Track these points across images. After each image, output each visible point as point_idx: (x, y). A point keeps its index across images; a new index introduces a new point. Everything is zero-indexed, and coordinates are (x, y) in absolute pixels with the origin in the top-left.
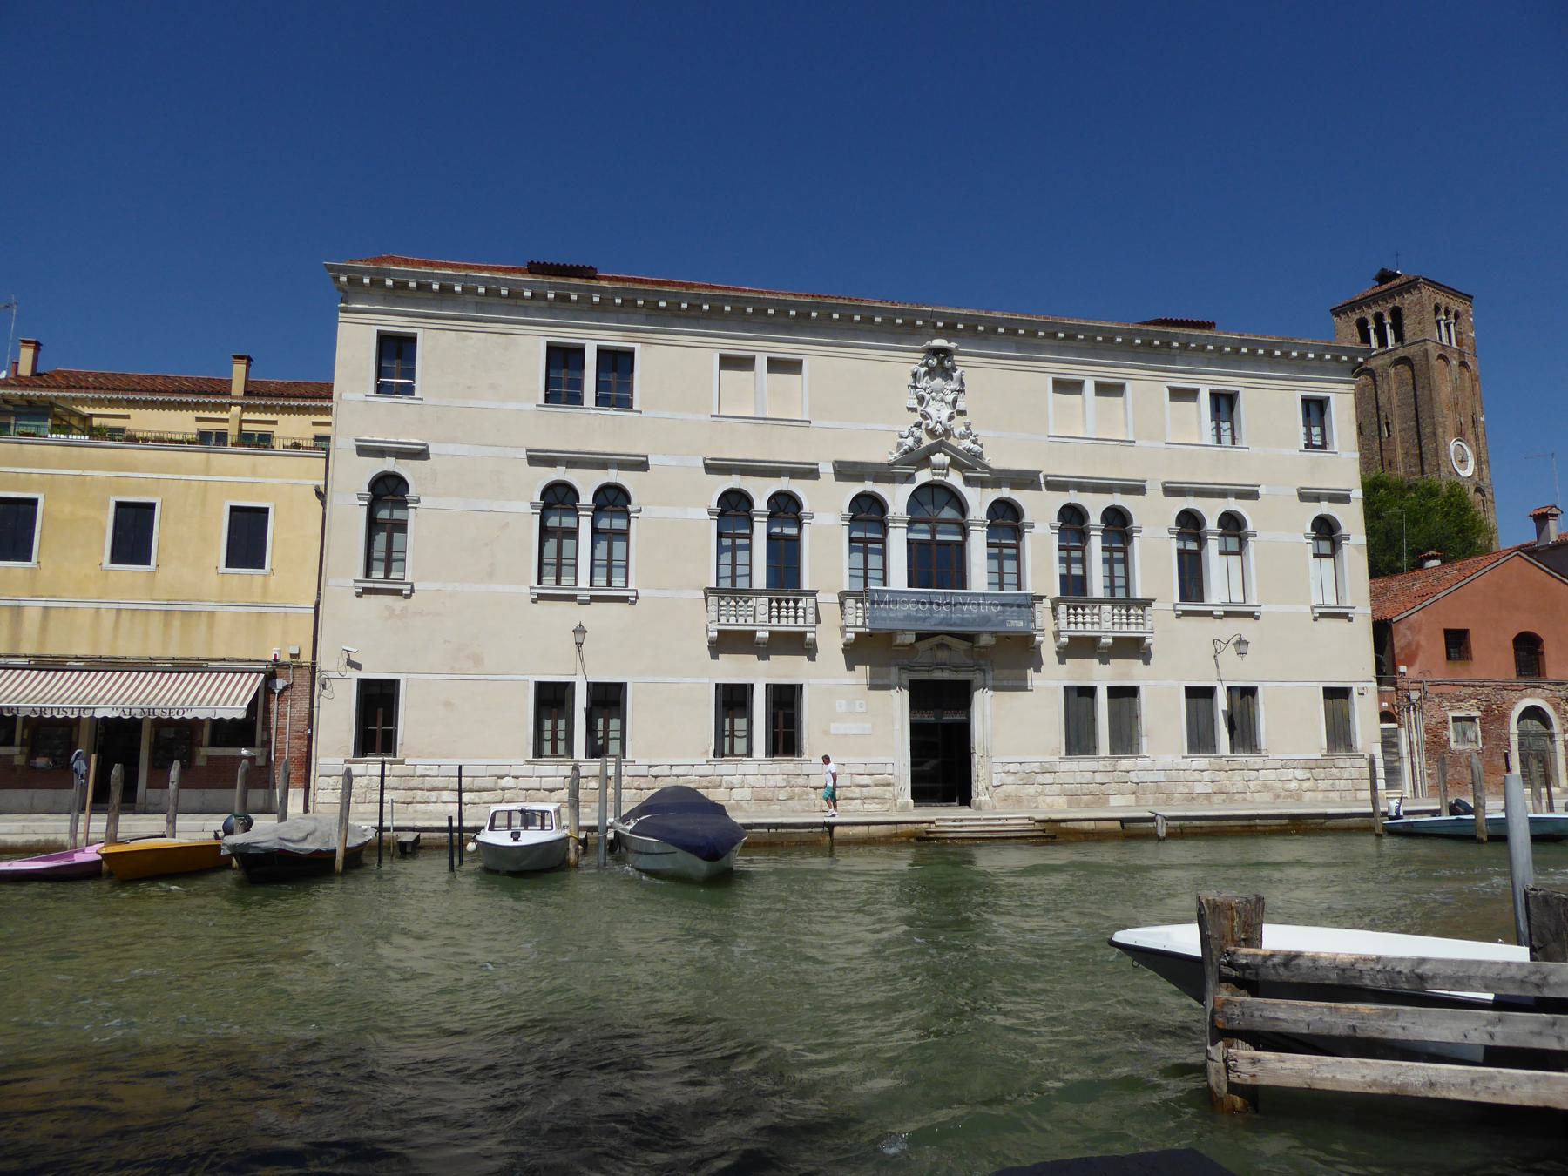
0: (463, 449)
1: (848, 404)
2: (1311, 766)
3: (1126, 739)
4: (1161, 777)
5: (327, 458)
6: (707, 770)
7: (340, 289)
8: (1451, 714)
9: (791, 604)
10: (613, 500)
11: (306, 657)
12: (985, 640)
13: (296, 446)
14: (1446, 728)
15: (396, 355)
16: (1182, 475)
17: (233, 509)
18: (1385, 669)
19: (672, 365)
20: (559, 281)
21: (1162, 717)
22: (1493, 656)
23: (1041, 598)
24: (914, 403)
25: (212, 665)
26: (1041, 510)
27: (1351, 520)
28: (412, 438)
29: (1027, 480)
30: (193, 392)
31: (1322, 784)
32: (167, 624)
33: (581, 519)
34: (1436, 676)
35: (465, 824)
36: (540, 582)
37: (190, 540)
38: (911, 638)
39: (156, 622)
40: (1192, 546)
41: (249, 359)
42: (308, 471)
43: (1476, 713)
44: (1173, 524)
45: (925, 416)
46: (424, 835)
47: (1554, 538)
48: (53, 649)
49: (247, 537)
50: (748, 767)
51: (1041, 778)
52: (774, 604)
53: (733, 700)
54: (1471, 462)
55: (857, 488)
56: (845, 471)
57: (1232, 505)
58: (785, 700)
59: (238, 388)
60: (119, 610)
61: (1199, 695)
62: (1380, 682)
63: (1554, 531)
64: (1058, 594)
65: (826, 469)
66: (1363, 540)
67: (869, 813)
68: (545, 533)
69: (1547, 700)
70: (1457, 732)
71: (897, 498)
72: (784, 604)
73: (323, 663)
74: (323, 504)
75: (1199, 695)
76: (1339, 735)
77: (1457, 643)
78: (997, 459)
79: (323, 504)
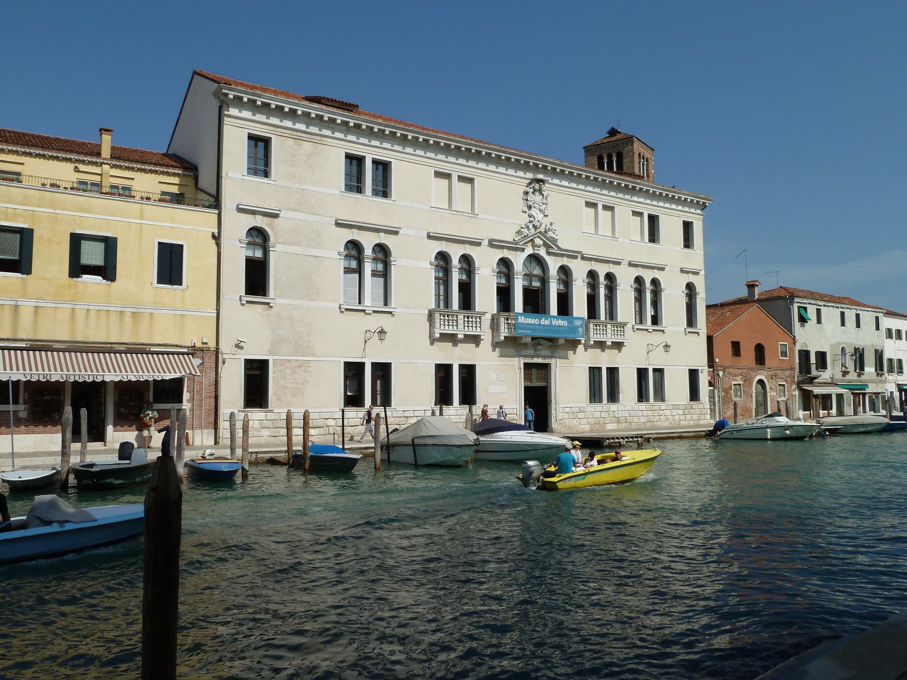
3: (613, 396)
4: (626, 414)
8: (733, 383)
10: (382, 251)
11: (212, 345)
12: (562, 341)
13: (148, 199)
15: (260, 146)
16: (636, 259)
17: (182, 246)
19: (412, 170)
20: (333, 106)
21: (628, 384)
22: (748, 352)
23: (484, 313)
24: (526, 209)
25: (153, 349)
26: (580, 271)
28: (270, 205)
29: (573, 255)
31: (688, 417)
34: (728, 364)
35: (346, 447)
37: (137, 263)
40: (259, 254)
42: (204, 220)
43: (741, 382)
44: (342, 249)
46: (259, 456)
47: (757, 297)
48: (44, 334)
49: (170, 265)
51: (579, 415)
56: (492, 244)
58: (468, 372)
59: (106, 152)
61: (642, 374)
64: (433, 307)
65: (486, 243)
71: (518, 260)
73: (223, 348)
74: (218, 245)
76: (694, 395)
77: (736, 347)
78: (564, 244)
79: (218, 245)
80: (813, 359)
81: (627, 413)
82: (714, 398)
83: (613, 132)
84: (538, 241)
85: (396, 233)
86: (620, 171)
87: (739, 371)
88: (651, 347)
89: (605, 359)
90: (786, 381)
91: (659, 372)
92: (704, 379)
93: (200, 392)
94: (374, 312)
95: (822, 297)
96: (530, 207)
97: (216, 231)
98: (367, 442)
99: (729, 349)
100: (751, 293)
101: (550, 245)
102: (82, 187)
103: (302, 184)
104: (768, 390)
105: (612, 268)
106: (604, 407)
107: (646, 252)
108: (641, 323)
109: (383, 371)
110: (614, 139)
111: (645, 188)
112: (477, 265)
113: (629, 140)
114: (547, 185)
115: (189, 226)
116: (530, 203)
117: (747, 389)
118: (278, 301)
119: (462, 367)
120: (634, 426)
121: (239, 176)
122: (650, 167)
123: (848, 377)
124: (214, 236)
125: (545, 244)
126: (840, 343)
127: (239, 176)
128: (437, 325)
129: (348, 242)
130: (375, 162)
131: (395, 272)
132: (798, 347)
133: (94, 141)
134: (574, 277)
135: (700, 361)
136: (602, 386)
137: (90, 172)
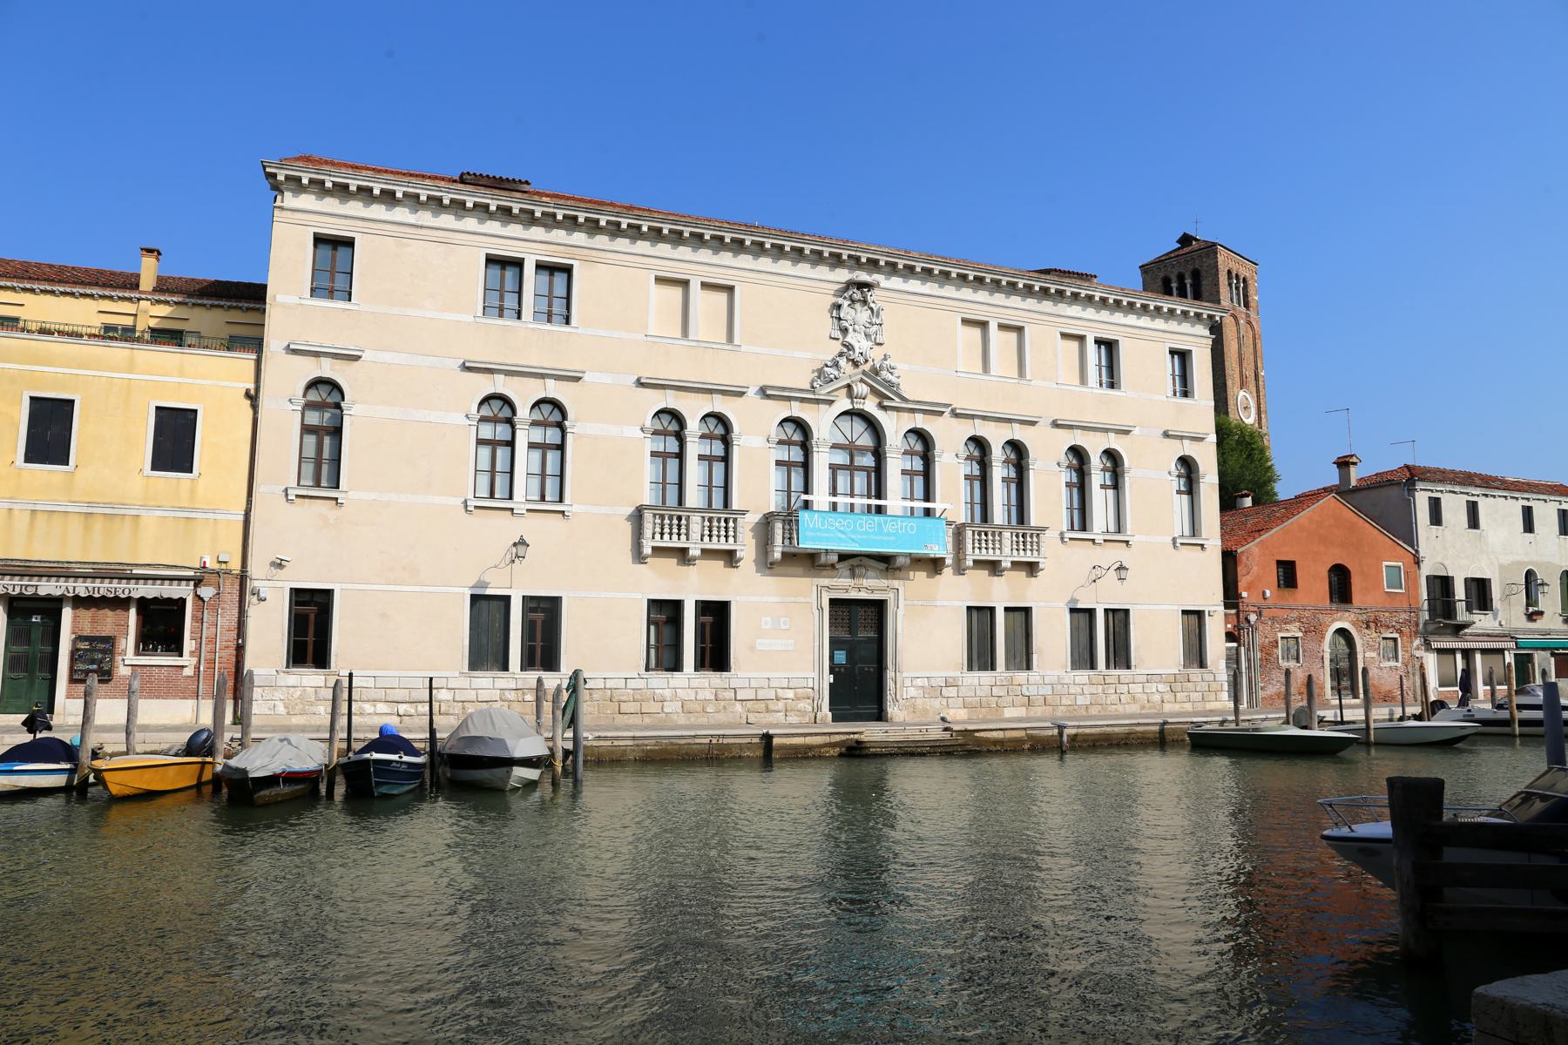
2: (1173, 682)
3: (1023, 657)
4: (1047, 691)
5: (258, 362)
6: (641, 684)
8: (1280, 635)
10: (554, 412)
11: (235, 565)
12: (900, 561)
18: (1231, 595)
19: (619, 283)
20: (495, 189)
21: (1053, 636)
22: (1314, 582)
24: (838, 334)
26: (950, 441)
27: (1207, 460)
29: (934, 411)
30: (97, 284)
32: (87, 528)
33: (522, 434)
37: (112, 440)
39: (76, 524)
42: (235, 368)
43: (1300, 634)
45: (850, 347)
47: (1353, 483)
49: (174, 440)
50: (677, 679)
51: (948, 692)
53: (665, 614)
54: (1253, 411)
57: (553, 390)
58: (716, 615)
59: (147, 283)
60: (33, 512)
61: (1083, 616)
62: (1226, 607)
63: (1355, 474)
64: (647, 496)
65: (752, 391)
67: (791, 725)
69: (1354, 624)
71: (823, 423)
74: (255, 407)
75: (1083, 616)
76: (1196, 654)
77: (1288, 574)
79: (255, 407)
80: (1460, 592)
81: (1053, 690)
82: (1238, 662)
83: (1186, 240)
84: (861, 389)
85: (1127, 432)
86: (1197, 296)
87: (1295, 614)
88: (1098, 572)
89: (1001, 593)
90: (1400, 632)
92: (1215, 629)
93: (213, 640)
95: (1467, 479)
96: (845, 331)
97: (252, 386)
98: (825, 724)
99: (1272, 574)
100: (1345, 477)
101: (886, 393)
102: (110, 333)
103: (412, 305)
104: (1359, 648)
105: (1019, 433)
106: (690, 681)
107: (1093, 403)
108: (1084, 528)
109: (1119, 619)
110: (1186, 250)
111: (1083, 293)
112: (1126, 463)
113: (1211, 248)
114: (876, 292)
115: (205, 379)
116: (845, 324)
117: (1312, 645)
121: (470, 318)
122: (1251, 291)
123: (1539, 624)
124: (247, 395)
125: (874, 391)
126: (1520, 563)
127: (296, 300)
128: (648, 532)
130: (1099, 342)
131: (1128, 480)
132: (1426, 570)
133: (128, 269)
134: (1202, 470)
135: (1210, 597)
136: (992, 638)
137: (120, 311)
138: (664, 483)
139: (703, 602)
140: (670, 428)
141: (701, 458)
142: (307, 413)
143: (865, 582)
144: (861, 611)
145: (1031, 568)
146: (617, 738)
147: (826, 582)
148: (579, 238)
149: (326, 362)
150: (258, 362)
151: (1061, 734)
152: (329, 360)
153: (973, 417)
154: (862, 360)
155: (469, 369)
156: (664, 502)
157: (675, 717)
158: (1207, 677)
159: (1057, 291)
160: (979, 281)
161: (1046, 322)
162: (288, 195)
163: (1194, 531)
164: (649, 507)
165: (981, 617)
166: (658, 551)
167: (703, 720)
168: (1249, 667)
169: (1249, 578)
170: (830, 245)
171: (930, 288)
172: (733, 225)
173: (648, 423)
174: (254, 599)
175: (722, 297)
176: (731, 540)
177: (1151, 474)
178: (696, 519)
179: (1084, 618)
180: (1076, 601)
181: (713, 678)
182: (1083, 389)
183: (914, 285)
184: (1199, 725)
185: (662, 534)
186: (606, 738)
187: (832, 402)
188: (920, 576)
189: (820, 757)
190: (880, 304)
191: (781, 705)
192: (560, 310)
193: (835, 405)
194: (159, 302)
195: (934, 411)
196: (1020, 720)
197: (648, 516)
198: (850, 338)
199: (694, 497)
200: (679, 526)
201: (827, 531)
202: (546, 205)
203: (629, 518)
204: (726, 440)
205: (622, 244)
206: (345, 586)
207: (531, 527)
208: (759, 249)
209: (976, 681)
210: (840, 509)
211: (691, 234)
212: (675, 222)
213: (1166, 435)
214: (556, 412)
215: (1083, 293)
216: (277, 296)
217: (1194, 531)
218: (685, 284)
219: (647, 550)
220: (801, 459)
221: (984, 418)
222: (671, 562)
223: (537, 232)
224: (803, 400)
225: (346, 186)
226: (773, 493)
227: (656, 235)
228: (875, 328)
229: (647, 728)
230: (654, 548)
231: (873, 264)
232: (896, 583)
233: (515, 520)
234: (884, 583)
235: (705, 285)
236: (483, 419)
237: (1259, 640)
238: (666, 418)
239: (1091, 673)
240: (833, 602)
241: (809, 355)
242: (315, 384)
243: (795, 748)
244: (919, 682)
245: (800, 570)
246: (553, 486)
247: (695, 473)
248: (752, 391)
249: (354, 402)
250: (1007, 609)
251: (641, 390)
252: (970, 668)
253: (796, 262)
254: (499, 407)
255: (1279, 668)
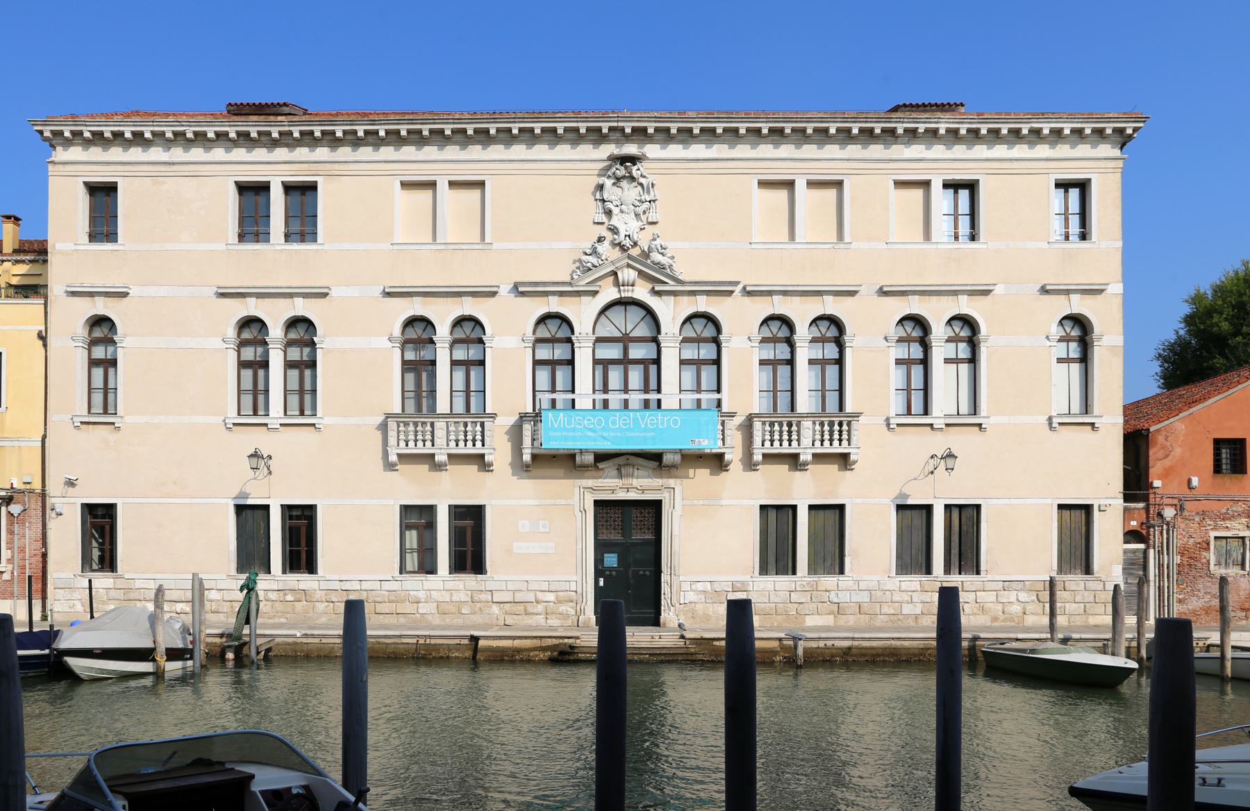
0: (162, 291)
1: (527, 220)
4: (865, 597)
5: (46, 305)
6: (394, 586)
7: (46, 139)
8: (1213, 534)
9: (411, 428)
11: (37, 486)
12: (667, 459)
14: (1208, 549)
18: (1136, 483)
19: (363, 193)
20: (257, 117)
21: (872, 538)
24: (604, 218)
26: (741, 323)
28: (114, 282)
29: (722, 291)
36: (89, 412)
38: (590, 458)
41: (17, 219)
45: (614, 230)
52: (402, 428)
53: (417, 518)
55: (766, 307)
57: (831, 306)
58: (470, 520)
62: (1127, 498)
65: (504, 290)
66: (1119, 340)
68: (93, 363)
70: (1218, 554)
71: (583, 314)
72: (420, 428)
74: (45, 346)
79: (45, 346)
82: (1145, 567)
84: (627, 275)
89: (803, 490)
91: (307, 513)
93: (22, 550)
94: (947, 425)
96: (609, 213)
97: (43, 328)
101: (658, 277)
106: (445, 584)
111: (921, 128)
118: (128, 419)
119: (458, 512)
120: (880, 621)
121: (222, 247)
127: (222, 247)
128: (392, 440)
129: (1064, 318)
130: (953, 186)
138: (775, 391)
139: (456, 507)
140: (829, 334)
141: (812, 362)
142: (289, 350)
143: (635, 482)
144: (635, 513)
145: (844, 460)
146: (324, 636)
147: (590, 483)
148: (322, 153)
149: (100, 301)
150: (46, 305)
151: (796, 647)
152: (254, 299)
153: (770, 293)
154: (627, 243)
155: (886, 294)
156: (824, 408)
157: (430, 617)
158: (1092, 585)
159: (1032, 131)
160: (777, 133)
161: (870, 171)
162: (59, 149)
163: (1086, 407)
164: (758, 415)
165: (777, 519)
166: (768, 457)
167: (459, 621)
168: (1160, 575)
169: (1167, 463)
170: (586, 120)
171: (719, 150)
172: (403, 117)
173: (397, 331)
174: (53, 514)
175: (831, 193)
176: (794, 443)
177: (1022, 342)
178: (807, 424)
179: (919, 518)
180: (907, 496)
181: (468, 581)
182: (926, 246)
183: (698, 150)
184: (1002, 641)
185: (822, 441)
186: (313, 636)
187: (597, 292)
188: (702, 474)
189: (529, 661)
190: (651, 179)
191: (540, 608)
192: (303, 226)
193: (598, 296)
194: (17, 262)
195: (722, 291)
196: (828, 629)
197: (757, 425)
198: (615, 221)
199: (806, 402)
200: (790, 433)
201: (574, 430)
202: (281, 124)
203: (379, 428)
204: (973, 343)
205: (366, 152)
206: (126, 500)
207: (957, 441)
208: (507, 138)
209: (770, 586)
210: (558, 406)
211: (748, 130)
212: (411, 121)
213: (1044, 291)
214: (784, 328)
215: (921, 128)
216: (57, 246)
217: (1086, 407)
218: (789, 185)
219: (758, 457)
220: (921, 356)
221: (785, 293)
222: (783, 468)
223: (281, 153)
224: (561, 294)
225: (713, 130)
226: (893, 392)
227: (395, 139)
228: (646, 205)
229: (280, 626)
230: (764, 455)
231: (640, 134)
232: (672, 482)
233: (939, 435)
234: (657, 482)
235: (452, 184)
236: (685, 340)
237: (1178, 540)
238: (824, 325)
239: (924, 578)
240: (598, 503)
241: (568, 245)
242: (411, 322)
243: (503, 651)
244: (700, 586)
245: (561, 472)
246: (304, 397)
247: (806, 378)
248: (504, 290)
249: (125, 336)
250: (811, 507)
251: (1047, 297)
252: (764, 570)
253: (821, 144)
254: (418, 329)
255: (1211, 576)
